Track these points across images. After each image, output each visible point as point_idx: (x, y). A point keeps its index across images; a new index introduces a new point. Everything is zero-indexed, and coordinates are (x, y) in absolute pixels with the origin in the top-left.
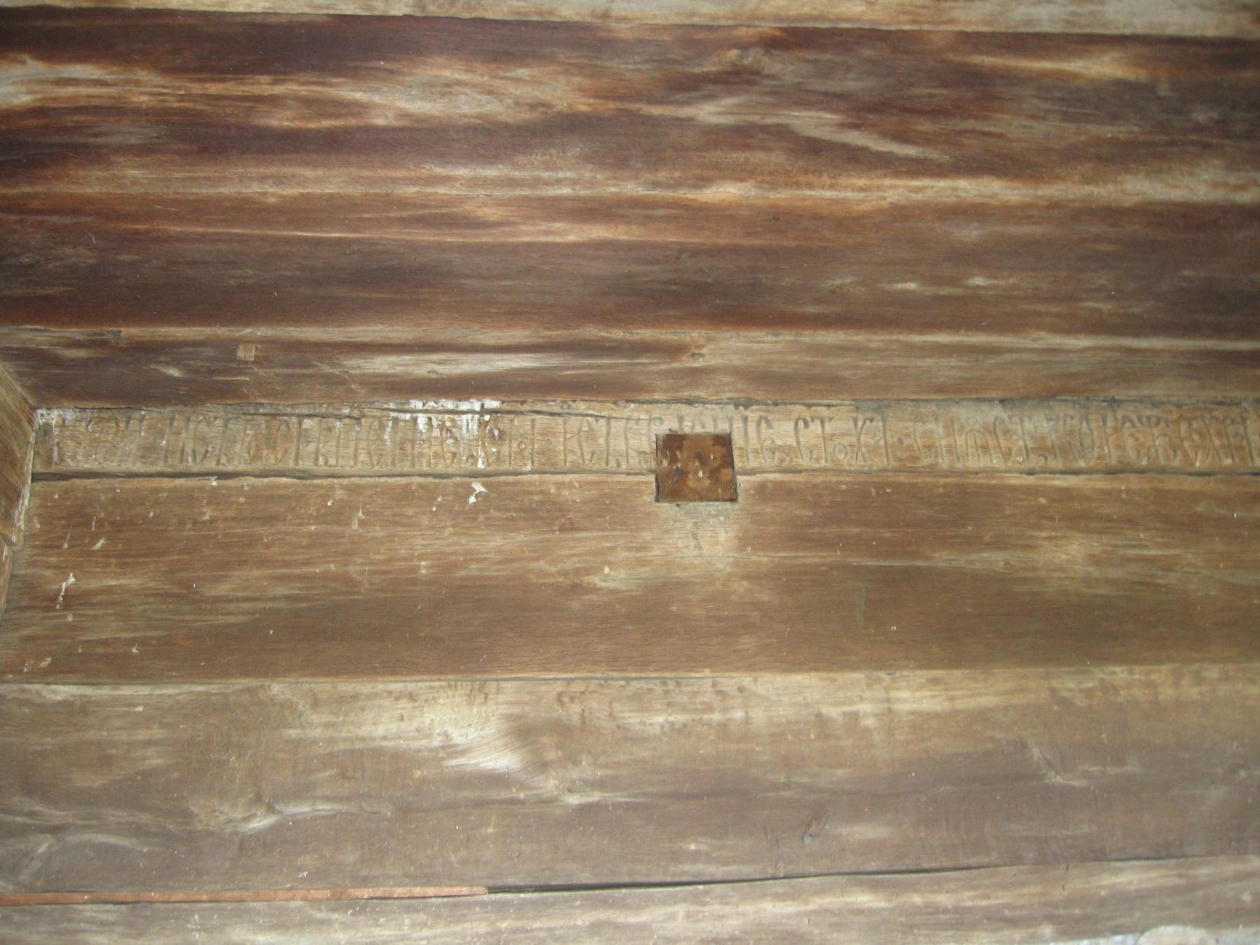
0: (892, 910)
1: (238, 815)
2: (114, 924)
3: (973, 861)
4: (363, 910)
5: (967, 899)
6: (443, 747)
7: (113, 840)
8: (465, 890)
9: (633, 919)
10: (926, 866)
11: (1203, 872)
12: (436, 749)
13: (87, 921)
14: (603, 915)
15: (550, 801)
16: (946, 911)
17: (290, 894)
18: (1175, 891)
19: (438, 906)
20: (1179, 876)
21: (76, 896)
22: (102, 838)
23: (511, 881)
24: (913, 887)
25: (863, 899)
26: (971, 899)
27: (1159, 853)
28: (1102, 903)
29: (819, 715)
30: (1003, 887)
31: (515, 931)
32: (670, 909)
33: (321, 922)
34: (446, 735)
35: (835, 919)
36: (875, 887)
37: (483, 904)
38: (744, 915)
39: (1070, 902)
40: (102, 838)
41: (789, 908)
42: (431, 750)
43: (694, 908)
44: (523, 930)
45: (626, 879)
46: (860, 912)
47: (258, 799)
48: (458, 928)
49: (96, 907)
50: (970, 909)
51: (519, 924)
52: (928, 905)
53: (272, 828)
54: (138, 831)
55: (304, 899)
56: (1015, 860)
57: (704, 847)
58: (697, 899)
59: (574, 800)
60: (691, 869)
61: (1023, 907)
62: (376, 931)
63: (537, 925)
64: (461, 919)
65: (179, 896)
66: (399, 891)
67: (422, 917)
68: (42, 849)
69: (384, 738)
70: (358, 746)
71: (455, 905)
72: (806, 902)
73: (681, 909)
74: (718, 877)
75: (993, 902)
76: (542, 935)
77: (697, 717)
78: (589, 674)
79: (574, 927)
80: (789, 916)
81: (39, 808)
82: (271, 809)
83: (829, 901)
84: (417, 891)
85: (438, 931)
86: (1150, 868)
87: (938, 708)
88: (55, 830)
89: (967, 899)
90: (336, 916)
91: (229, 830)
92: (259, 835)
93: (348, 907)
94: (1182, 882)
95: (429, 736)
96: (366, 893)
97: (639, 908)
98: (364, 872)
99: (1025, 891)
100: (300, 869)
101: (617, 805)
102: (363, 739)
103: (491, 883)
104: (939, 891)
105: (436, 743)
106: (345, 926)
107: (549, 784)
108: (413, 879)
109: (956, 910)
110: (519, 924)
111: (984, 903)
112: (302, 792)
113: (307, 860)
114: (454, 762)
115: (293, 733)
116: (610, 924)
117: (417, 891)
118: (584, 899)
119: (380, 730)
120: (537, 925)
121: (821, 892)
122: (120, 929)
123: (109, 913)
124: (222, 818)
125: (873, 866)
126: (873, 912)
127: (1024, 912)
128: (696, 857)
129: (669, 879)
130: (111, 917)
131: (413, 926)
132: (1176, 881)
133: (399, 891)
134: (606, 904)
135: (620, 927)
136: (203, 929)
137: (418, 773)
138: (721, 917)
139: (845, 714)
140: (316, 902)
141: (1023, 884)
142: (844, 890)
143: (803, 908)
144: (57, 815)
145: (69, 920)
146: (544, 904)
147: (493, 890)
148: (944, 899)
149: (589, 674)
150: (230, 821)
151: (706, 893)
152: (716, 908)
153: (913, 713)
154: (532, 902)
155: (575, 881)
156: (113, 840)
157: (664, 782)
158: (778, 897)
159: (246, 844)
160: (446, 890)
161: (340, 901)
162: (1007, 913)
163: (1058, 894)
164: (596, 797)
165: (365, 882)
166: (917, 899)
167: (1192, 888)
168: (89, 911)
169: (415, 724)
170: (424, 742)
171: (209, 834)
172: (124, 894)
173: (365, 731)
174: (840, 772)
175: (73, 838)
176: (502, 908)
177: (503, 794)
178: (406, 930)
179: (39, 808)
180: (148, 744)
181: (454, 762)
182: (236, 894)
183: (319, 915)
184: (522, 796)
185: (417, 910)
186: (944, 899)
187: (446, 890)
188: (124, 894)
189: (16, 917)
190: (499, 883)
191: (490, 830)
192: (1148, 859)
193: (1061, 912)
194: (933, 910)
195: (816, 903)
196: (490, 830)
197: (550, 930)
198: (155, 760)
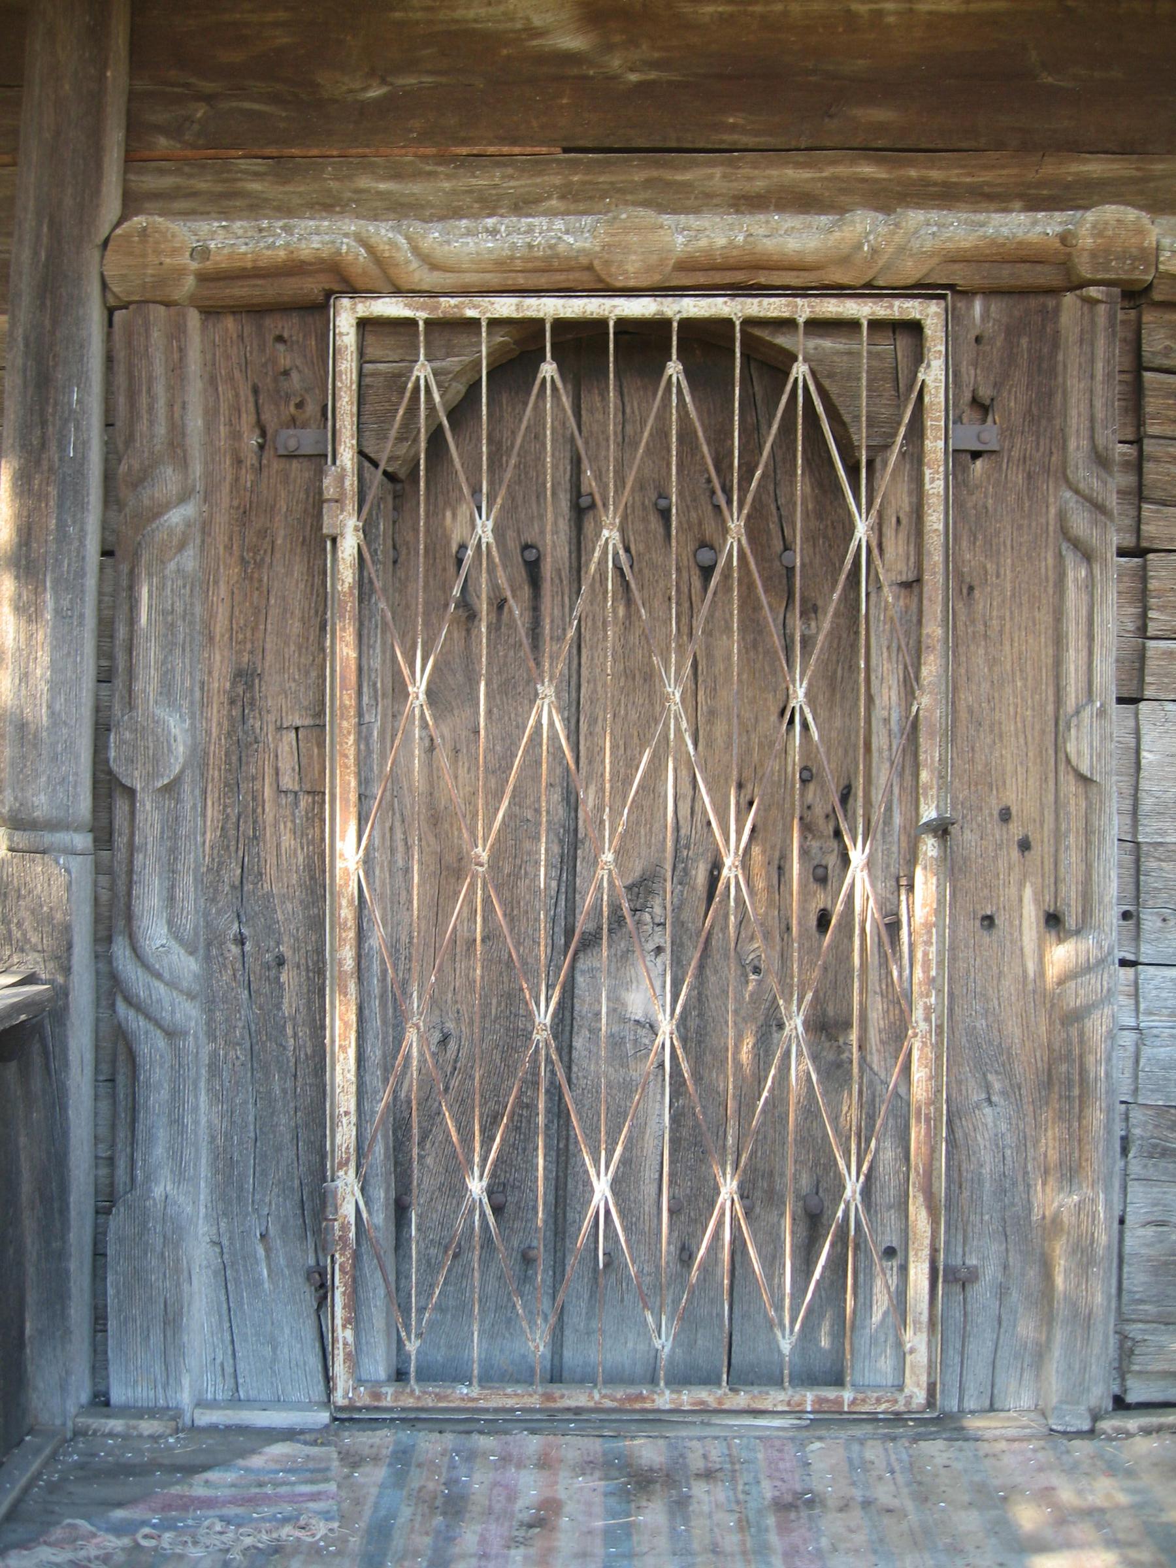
0: (890, 180)
1: (357, 85)
2: (265, 174)
3: (964, 145)
4: (462, 165)
5: (955, 175)
6: (525, 30)
7: (256, 106)
8: (544, 150)
9: (680, 177)
10: (923, 146)
11: (1159, 167)
12: (519, 31)
13: (241, 171)
14: (654, 173)
15: (614, 78)
16: (935, 184)
17: (403, 151)
18: (1133, 181)
19: (523, 162)
20: (1138, 169)
21: (233, 153)
22: (247, 105)
23: (581, 143)
24: (911, 164)
25: (868, 170)
26: (958, 175)
27: (1125, 149)
28: (1068, 186)
29: (849, 11)
30: (985, 167)
31: (584, 183)
32: (710, 171)
33: (430, 174)
34: (528, 19)
35: (844, 185)
36: (879, 162)
37: (558, 161)
38: (769, 177)
39: (1040, 184)
40: (247, 105)
41: (806, 174)
42: (515, 31)
43: (729, 170)
44: (590, 183)
45: (674, 144)
46: (864, 180)
47: (372, 73)
48: (539, 180)
49: (249, 161)
50: (956, 184)
51: (588, 178)
52: (922, 179)
53: (385, 97)
54: (275, 99)
55: (416, 156)
56: (1000, 146)
57: (741, 121)
58: (731, 163)
59: (633, 77)
60: (729, 138)
61: (1000, 185)
62: (474, 181)
63: (601, 179)
64: (541, 173)
65: (315, 152)
66: (491, 150)
67: (510, 171)
68: (199, 115)
69: (475, 21)
70: (454, 27)
71: (537, 162)
72: (821, 170)
73: (718, 172)
74: (750, 146)
75: (975, 179)
76: (606, 187)
77: (741, 8)
78: (674, 390)
79: (632, 181)
80: (807, 181)
81: (193, 80)
82: (384, 82)
83: (842, 170)
84: (506, 149)
85: (522, 182)
86: (1113, 161)
87: (954, 9)
88: (209, 98)
89: (955, 175)
90: (440, 169)
91: (350, 98)
92: (377, 101)
93: (451, 162)
94: (1138, 174)
95: (512, 20)
96: (464, 150)
97: (685, 168)
98: (463, 134)
99: (1004, 172)
100: (411, 131)
101: (670, 83)
102: (457, 21)
103: (565, 144)
104: (931, 168)
105: (519, 25)
106: (449, 177)
107: (615, 62)
108: (502, 140)
109: (945, 184)
110: (588, 178)
111: (968, 180)
112: (410, 65)
113: (417, 123)
114: (535, 43)
115: (398, 15)
116: (660, 179)
117: (506, 149)
118: (640, 159)
119: (471, 14)
120: (601, 179)
121: (834, 162)
122: (269, 178)
123: (258, 165)
124: (345, 88)
125: (880, 144)
126: (876, 181)
127: (1000, 190)
128: (733, 128)
129: (710, 146)
130: (262, 169)
131: (503, 177)
132: (1135, 173)
133: (491, 150)
134: (658, 165)
135: (669, 184)
136: (336, 179)
137: (505, 52)
138: (750, 179)
139: (871, 11)
140: (425, 158)
141: (1003, 167)
142: (853, 162)
143: (818, 175)
144: (208, 87)
145: (229, 171)
146: (608, 163)
147: (566, 150)
148: (935, 174)
149: (674, 390)
150: (351, 91)
151: (739, 159)
152: (746, 171)
153: (930, 13)
154: (597, 161)
155: (634, 145)
156: (256, 106)
157: (881, 1540)
158: (798, 165)
159: (364, 110)
160: (528, 150)
161: (443, 159)
162: (986, 189)
163: (1031, 176)
164: (653, 75)
165: (464, 142)
166: (913, 173)
167: (1145, 180)
168: (243, 164)
169: (502, 8)
170: (509, 25)
171: (335, 101)
172: (271, 151)
173: (459, 13)
174: (860, 62)
175: (225, 105)
176: (574, 164)
177: (575, 71)
178: (497, 181)
179: (193, 80)
180: (276, 24)
181: (535, 43)
182: (360, 150)
183: (428, 168)
184: (591, 73)
185: (505, 165)
186: (935, 174)
187: (528, 150)
188: (271, 151)
189: (187, 169)
190: (572, 145)
191: (565, 101)
192: (1113, 153)
193: (1033, 191)
194: (926, 183)
195: (828, 172)
196: (565, 101)
197: (612, 183)
198: (283, 39)
